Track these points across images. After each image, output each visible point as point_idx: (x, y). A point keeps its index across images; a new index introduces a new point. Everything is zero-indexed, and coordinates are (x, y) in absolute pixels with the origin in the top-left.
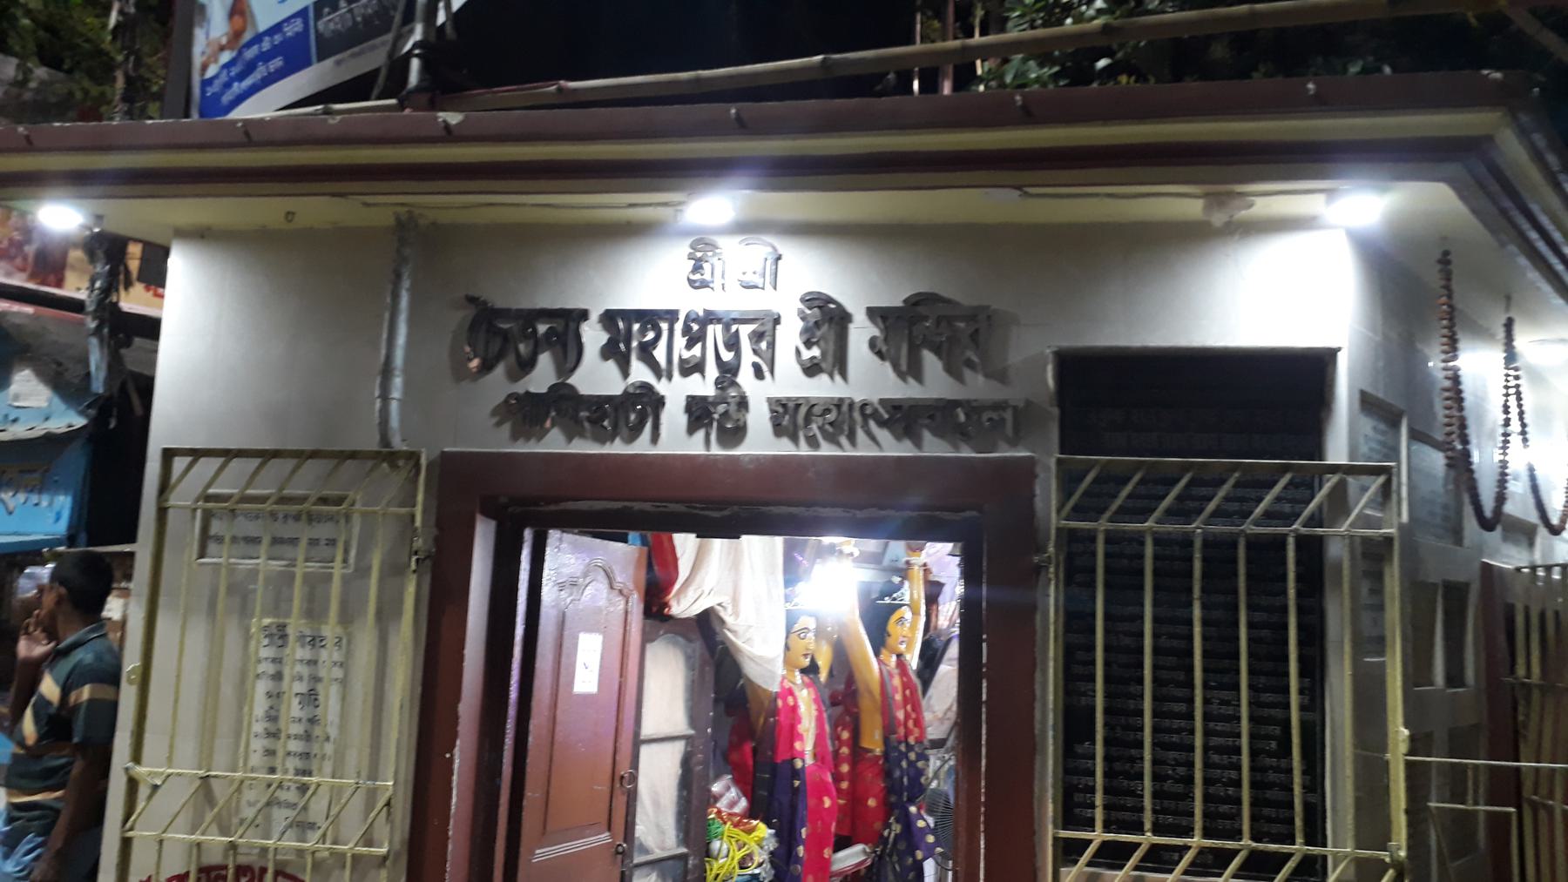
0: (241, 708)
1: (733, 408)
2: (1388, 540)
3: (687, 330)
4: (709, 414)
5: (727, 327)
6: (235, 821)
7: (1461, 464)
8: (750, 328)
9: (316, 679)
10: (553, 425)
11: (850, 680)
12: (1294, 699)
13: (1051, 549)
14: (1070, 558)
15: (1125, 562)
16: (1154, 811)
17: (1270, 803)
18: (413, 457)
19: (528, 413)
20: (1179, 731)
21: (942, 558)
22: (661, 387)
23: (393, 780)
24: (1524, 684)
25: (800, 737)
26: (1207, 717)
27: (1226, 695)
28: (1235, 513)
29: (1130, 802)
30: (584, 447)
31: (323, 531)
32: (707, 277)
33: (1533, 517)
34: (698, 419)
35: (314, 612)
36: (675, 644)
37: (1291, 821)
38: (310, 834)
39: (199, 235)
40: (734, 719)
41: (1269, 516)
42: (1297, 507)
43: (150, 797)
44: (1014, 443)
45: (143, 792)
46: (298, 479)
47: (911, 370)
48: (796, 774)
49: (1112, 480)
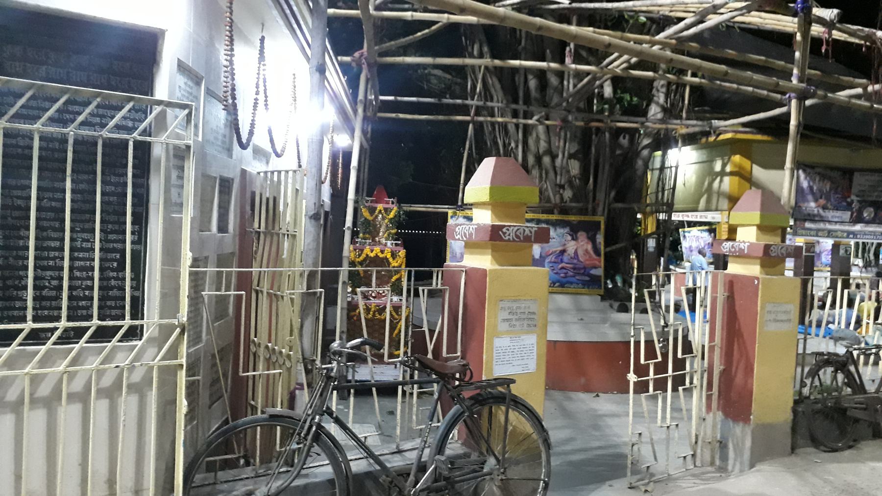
7: (232, 110)
12: (129, 237)
15: (20, 150)
16: (34, 309)
24: (257, 232)
26: (72, 250)
27: (85, 236)
29: (18, 304)
33: (268, 147)
37: (124, 307)
41: (118, 128)
42: (137, 124)
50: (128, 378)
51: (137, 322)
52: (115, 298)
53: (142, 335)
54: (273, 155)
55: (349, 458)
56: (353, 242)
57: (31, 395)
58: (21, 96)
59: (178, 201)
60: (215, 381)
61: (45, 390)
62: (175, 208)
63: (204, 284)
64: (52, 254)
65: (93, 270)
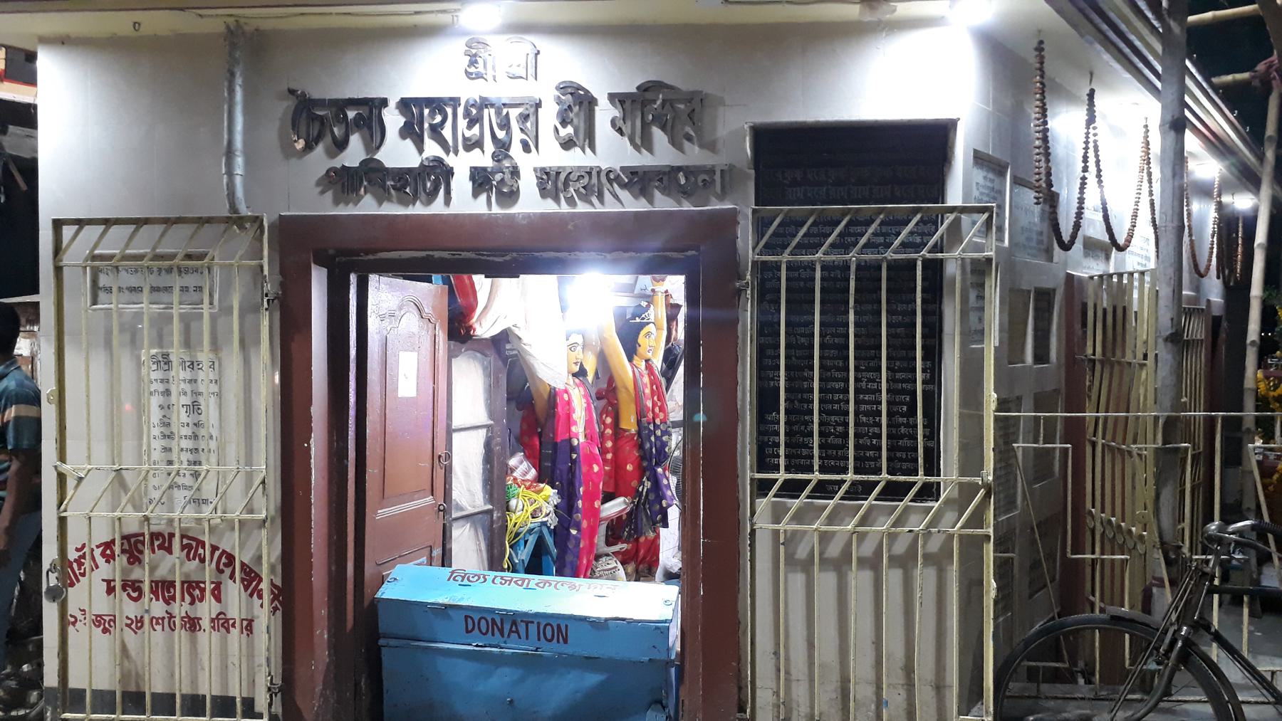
0: (140, 418)
1: (508, 176)
2: (989, 260)
3: (467, 114)
4: (489, 181)
5: (498, 113)
6: (145, 500)
7: (1050, 200)
8: (520, 110)
9: (196, 393)
10: (365, 193)
11: (611, 380)
13: (748, 277)
14: (762, 284)
15: (802, 284)
16: (820, 458)
17: (901, 449)
18: (257, 220)
19: (345, 183)
20: (839, 402)
21: (675, 285)
22: (450, 160)
23: (266, 461)
24: (1090, 360)
25: (575, 423)
26: (857, 391)
28: (880, 244)
29: (805, 452)
30: (392, 209)
31: (190, 280)
32: (481, 69)
34: (480, 185)
35: (188, 342)
36: (475, 358)
38: (204, 507)
39: (61, 42)
40: (529, 419)
41: (904, 245)
43: (77, 487)
44: (721, 198)
45: (71, 483)
46: (167, 243)
47: (644, 143)
48: (573, 449)
49: (792, 223)
50: (923, 546)
52: (906, 449)
53: (939, 495)
55: (1240, 699)
56: (1261, 364)
57: (821, 554)
59: (979, 328)
60: (1036, 565)
61: (834, 550)
62: (976, 338)
63: (1016, 433)
64: (836, 397)
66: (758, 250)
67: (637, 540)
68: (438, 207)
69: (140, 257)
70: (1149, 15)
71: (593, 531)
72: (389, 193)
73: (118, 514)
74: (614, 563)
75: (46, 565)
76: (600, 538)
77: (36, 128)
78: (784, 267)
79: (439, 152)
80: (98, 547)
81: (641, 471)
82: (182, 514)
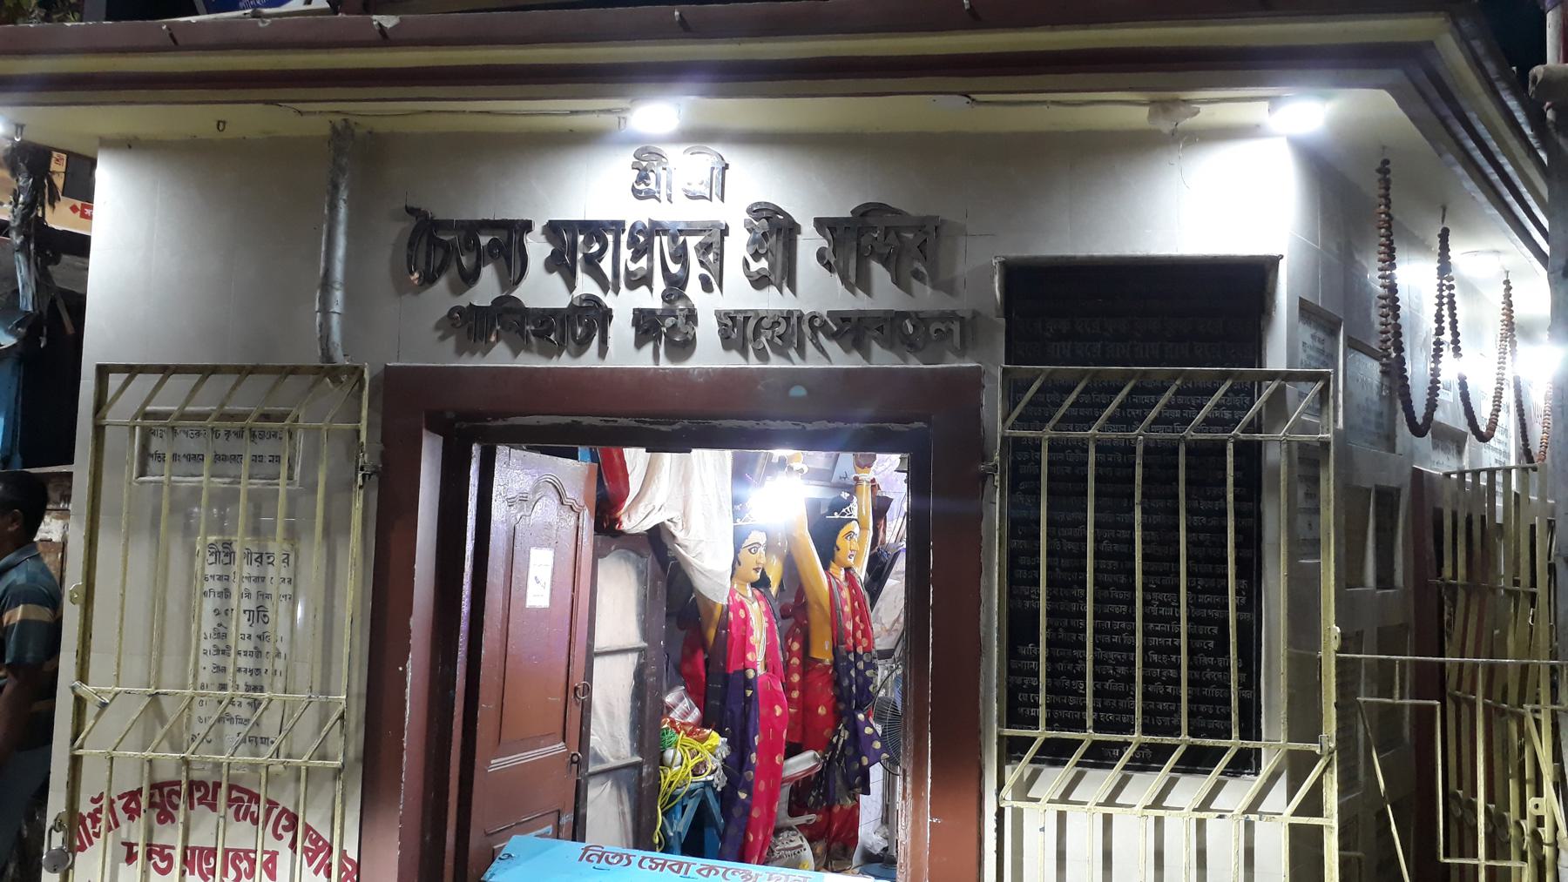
1: (681, 321)
2: (1325, 445)
3: (633, 242)
5: (674, 239)
6: (187, 737)
7: (1395, 373)
8: (699, 239)
9: (263, 595)
10: (498, 340)
11: (801, 593)
13: (997, 458)
16: (1095, 709)
19: (474, 326)
22: (609, 300)
25: (752, 648)
27: (1164, 596)
28: (1176, 420)
29: (1072, 700)
31: (265, 447)
32: (652, 186)
33: (1462, 425)
34: (646, 332)
36: (627, 559)
38: (263, 748)
39: (127, 145)
41: (1209, 422)
42: (1237, 414)
43: (98, 716)
44: (961, 352)
45: (91, 710)
46: (238, 398)
47: (859, 282)
48: (748, 683)
51: (1251, 744)
53: (1259, 766)
54: (1472, 438)
58: (1070, 390)
59: (1310, 536)
65: (1179, 653)
66: (1009, 423)
67: (829, 809)
68: (589, 359)
69: (202, 416)
70: (1528, 131)
71: (772, 796)
72: (528, 341)
73: (148, 754)
74: (798, 840)
75: (50, 822)
76: (781, 806)
77: (87, 256)
78: (1045, 446)
79: (595, 290)
80: (120, 798)
81: (837, 716)
82: (236, 758)
